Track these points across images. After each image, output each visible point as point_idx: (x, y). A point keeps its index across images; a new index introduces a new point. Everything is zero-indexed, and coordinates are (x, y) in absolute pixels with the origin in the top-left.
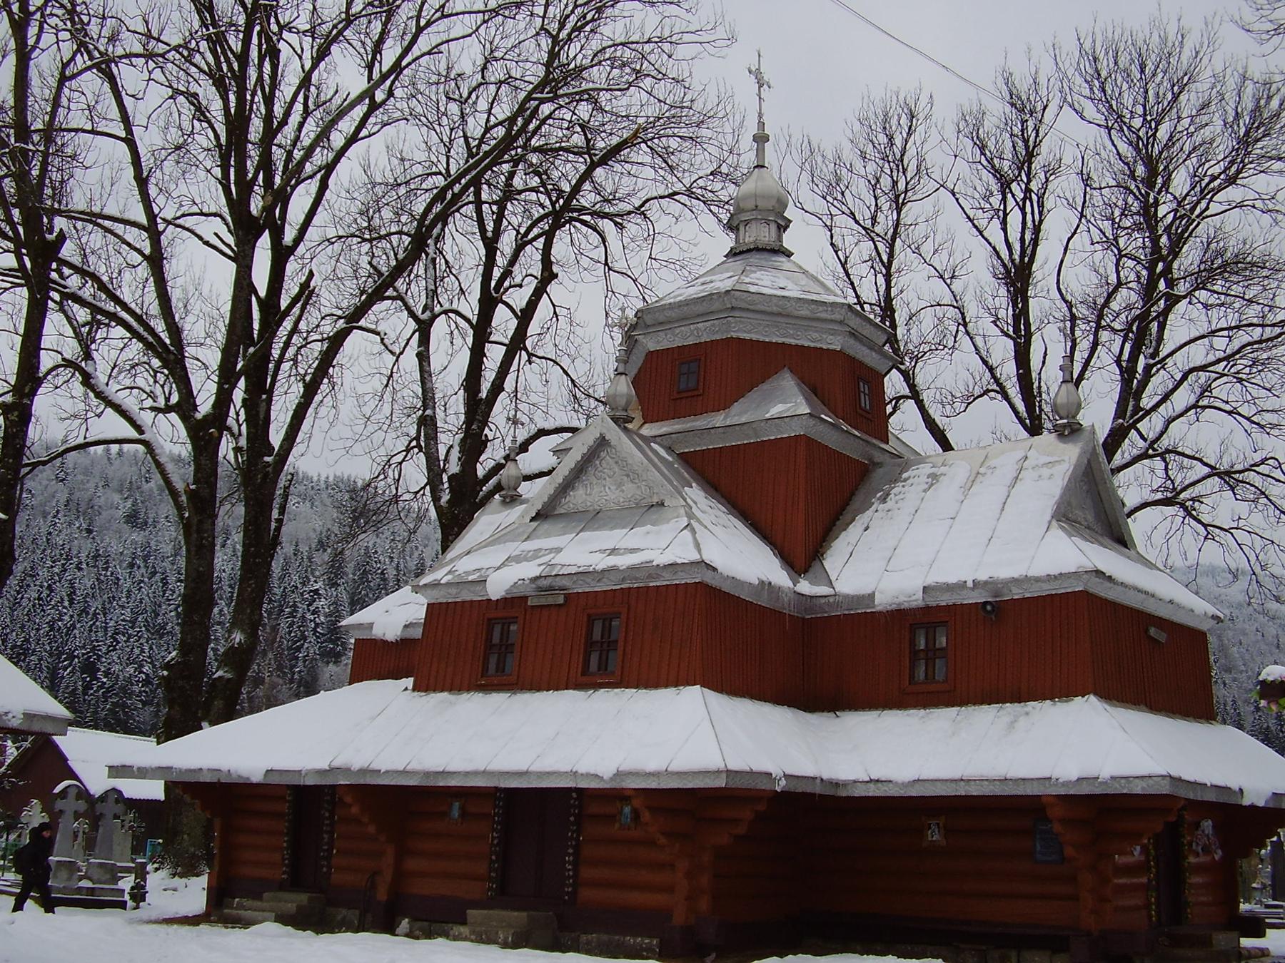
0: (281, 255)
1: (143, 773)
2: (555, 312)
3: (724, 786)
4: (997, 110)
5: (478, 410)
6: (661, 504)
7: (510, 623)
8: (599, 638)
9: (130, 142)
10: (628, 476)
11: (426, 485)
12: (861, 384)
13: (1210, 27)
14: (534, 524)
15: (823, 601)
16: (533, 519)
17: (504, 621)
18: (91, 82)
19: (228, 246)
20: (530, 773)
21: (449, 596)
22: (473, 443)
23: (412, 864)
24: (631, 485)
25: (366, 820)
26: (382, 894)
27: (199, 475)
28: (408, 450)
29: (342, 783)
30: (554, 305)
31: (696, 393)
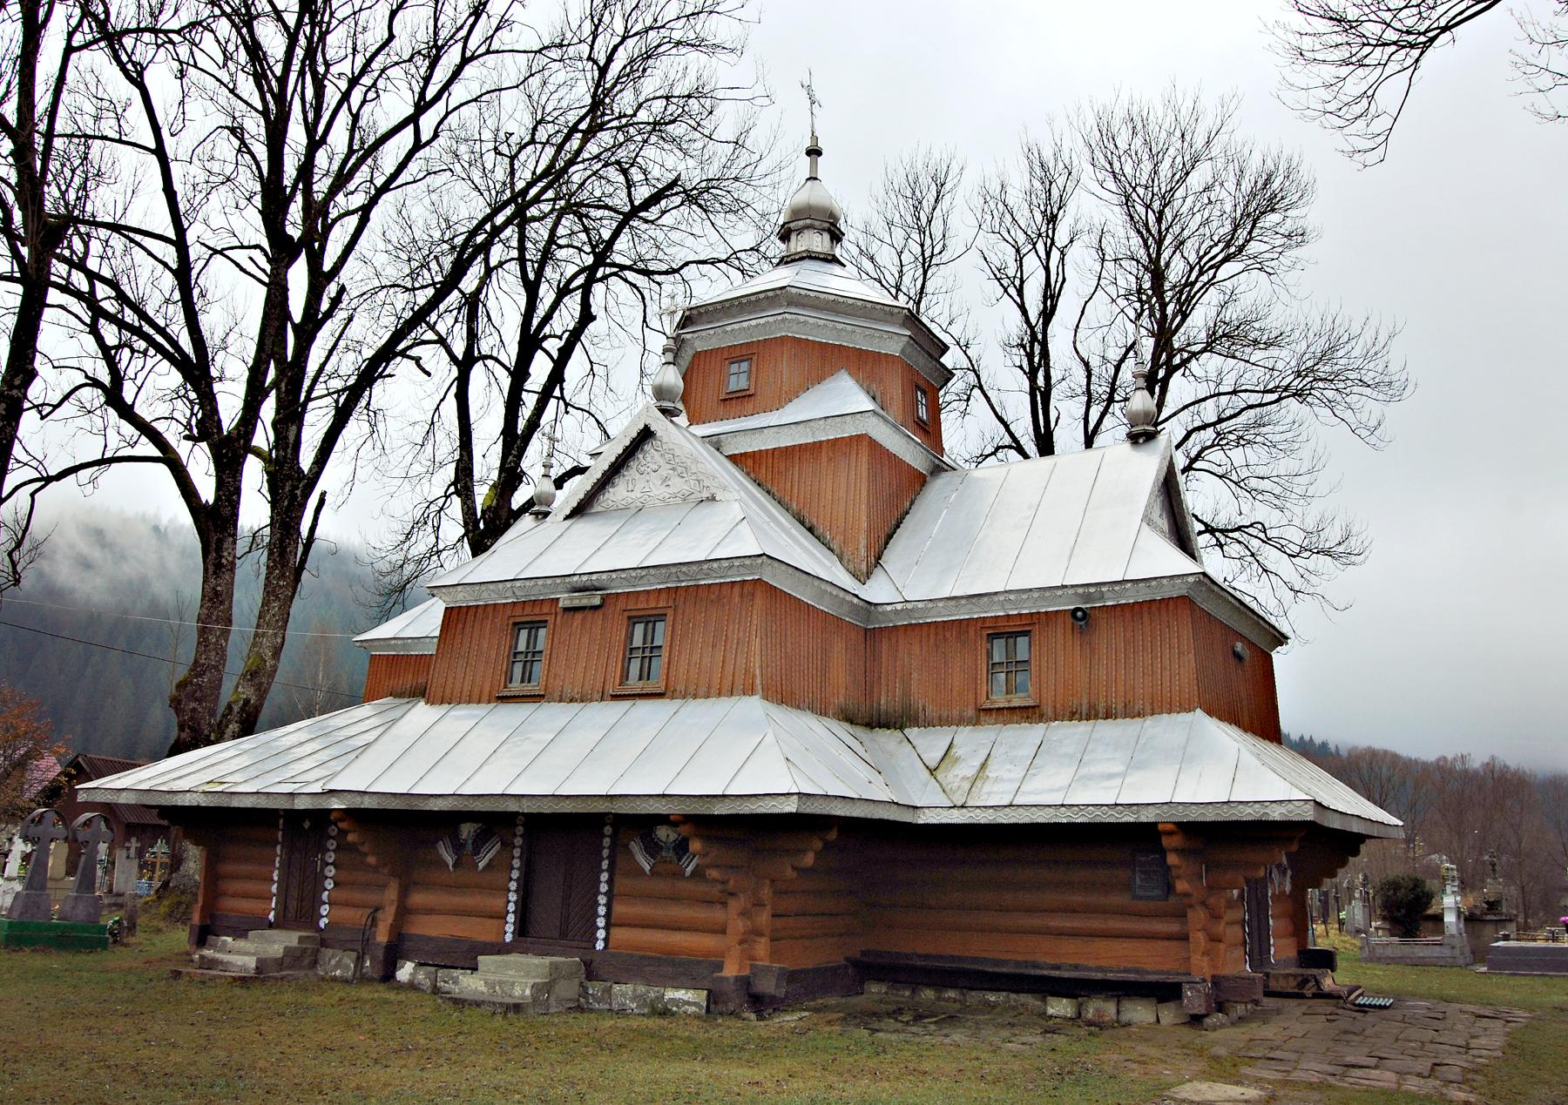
0: (319, 281)
2: (592, 369)
3: (794, 811)
4: (1019, 183)
5: (514, 441)
6: (713, 499)
7: (538, 628)
8: (640, 645)
9: (160, 152)
10: (674, 469)
11: (463, 537)
12: (919, 393)
13: (1226, 108)
14: (569, 522)
15: (889, 608)
16: (567, 518)
17: (531, 625)
18: (97, 60)
19: (264, 271)
22: (511, 476)
23: (418, 898)
24: (678, 479)
25: (365, 849)
26: (382, 937)
27: (221, 493)
28: (447, 497)
29: (336, 807)
30: (591, 362)
31: (748, 393)
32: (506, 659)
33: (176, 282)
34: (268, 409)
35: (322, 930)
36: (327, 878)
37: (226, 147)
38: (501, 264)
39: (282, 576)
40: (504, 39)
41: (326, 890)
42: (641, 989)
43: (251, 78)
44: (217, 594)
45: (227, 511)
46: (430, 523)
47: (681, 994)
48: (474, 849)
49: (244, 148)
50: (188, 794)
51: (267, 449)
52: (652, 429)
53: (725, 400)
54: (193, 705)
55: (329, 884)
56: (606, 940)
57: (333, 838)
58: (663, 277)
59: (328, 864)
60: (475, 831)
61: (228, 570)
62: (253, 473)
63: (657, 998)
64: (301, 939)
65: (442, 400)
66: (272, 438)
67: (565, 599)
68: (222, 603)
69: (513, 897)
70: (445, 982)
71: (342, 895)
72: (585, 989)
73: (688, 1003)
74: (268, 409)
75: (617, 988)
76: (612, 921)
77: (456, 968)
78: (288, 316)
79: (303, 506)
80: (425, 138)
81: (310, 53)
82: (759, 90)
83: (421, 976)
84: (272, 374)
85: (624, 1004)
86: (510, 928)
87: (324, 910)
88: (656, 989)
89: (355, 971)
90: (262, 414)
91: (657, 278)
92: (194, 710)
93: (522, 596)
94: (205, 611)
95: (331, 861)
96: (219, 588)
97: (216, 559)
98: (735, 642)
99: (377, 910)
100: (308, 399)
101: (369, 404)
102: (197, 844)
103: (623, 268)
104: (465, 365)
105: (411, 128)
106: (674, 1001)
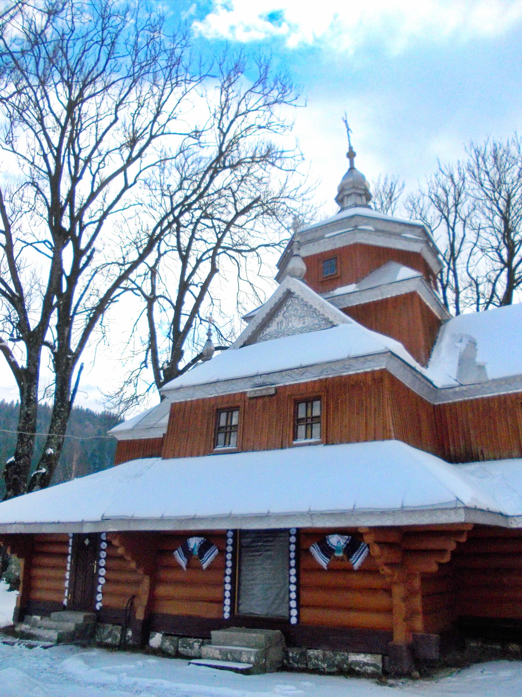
0: (78, 253)
1: (487, 674)
2: (212, 302)
20: (270, 516)
21: (187, 396)
23: (162, 590)
26: (140, 615)
31: (336, 276)
32: (213, 431)
33: (5, 252)
34: (54, 320)
35: (98, 611)
36: (100, 576)
37: (30, 191)
38: (165, 252)
39: (62, 406)
40: (171, 126)
41: (100, 584)
42: (329, 654)
43: (42, 157)
44: (28, 415)
45: (33, 370)
46: (133, 382)
47: (361, 658)
48: (199, 555)
49: (39, 191)
50: (14, 526)
51: (53, 342)
52: (292, 291)
53: (322, 281)
54: (15, 476)
55: (102, 581)
56: (298, 616)
57: (104, 550)
58: (247, 253)
59: (101, 567)
60: (200, 543)
61: (34, 402)
62: (46, 354)
63: (343, 660)
64: (85, 618)
65: (138, 320)
66: (56, 336)
67: (250, 392)
68: (31, 420)
69: (228, 587)
70: (184, 647)
71: (110, 588)
72: (287, 653)
73: (367, 664)
74: (54, 320)
75: (311, 652)
76: (302, 603)
77: (191, 637)
78: (62, 272)
79: (72, 369)
80: (130, 182)
81: (71, 141)
82: (297, 152)
83: (167, 644)
84: (55, 300)
85: (318, 665)
86: (227, 609)
87: (99, 597)
88: (342, 653)
89: (121, 639)
90: (50, 324)
91: (243, 253)
92: (15, 479)
93: (221, 392)
94: (21, 425)
95: (102, 565)
96: (29, 412)
97: (27, 396)
98: (373, 410)
99: (134, 597)
100: (75, 313)
101: (101, 322)
102: (19, 556)
103: (228, 248)
104: (151, 300)
105: (122, 174)
106: (358, 663)
